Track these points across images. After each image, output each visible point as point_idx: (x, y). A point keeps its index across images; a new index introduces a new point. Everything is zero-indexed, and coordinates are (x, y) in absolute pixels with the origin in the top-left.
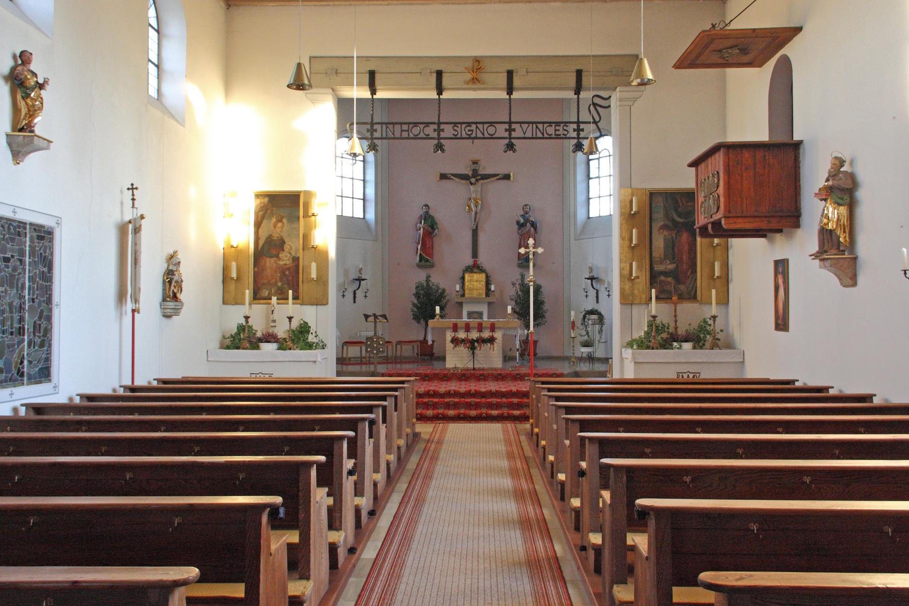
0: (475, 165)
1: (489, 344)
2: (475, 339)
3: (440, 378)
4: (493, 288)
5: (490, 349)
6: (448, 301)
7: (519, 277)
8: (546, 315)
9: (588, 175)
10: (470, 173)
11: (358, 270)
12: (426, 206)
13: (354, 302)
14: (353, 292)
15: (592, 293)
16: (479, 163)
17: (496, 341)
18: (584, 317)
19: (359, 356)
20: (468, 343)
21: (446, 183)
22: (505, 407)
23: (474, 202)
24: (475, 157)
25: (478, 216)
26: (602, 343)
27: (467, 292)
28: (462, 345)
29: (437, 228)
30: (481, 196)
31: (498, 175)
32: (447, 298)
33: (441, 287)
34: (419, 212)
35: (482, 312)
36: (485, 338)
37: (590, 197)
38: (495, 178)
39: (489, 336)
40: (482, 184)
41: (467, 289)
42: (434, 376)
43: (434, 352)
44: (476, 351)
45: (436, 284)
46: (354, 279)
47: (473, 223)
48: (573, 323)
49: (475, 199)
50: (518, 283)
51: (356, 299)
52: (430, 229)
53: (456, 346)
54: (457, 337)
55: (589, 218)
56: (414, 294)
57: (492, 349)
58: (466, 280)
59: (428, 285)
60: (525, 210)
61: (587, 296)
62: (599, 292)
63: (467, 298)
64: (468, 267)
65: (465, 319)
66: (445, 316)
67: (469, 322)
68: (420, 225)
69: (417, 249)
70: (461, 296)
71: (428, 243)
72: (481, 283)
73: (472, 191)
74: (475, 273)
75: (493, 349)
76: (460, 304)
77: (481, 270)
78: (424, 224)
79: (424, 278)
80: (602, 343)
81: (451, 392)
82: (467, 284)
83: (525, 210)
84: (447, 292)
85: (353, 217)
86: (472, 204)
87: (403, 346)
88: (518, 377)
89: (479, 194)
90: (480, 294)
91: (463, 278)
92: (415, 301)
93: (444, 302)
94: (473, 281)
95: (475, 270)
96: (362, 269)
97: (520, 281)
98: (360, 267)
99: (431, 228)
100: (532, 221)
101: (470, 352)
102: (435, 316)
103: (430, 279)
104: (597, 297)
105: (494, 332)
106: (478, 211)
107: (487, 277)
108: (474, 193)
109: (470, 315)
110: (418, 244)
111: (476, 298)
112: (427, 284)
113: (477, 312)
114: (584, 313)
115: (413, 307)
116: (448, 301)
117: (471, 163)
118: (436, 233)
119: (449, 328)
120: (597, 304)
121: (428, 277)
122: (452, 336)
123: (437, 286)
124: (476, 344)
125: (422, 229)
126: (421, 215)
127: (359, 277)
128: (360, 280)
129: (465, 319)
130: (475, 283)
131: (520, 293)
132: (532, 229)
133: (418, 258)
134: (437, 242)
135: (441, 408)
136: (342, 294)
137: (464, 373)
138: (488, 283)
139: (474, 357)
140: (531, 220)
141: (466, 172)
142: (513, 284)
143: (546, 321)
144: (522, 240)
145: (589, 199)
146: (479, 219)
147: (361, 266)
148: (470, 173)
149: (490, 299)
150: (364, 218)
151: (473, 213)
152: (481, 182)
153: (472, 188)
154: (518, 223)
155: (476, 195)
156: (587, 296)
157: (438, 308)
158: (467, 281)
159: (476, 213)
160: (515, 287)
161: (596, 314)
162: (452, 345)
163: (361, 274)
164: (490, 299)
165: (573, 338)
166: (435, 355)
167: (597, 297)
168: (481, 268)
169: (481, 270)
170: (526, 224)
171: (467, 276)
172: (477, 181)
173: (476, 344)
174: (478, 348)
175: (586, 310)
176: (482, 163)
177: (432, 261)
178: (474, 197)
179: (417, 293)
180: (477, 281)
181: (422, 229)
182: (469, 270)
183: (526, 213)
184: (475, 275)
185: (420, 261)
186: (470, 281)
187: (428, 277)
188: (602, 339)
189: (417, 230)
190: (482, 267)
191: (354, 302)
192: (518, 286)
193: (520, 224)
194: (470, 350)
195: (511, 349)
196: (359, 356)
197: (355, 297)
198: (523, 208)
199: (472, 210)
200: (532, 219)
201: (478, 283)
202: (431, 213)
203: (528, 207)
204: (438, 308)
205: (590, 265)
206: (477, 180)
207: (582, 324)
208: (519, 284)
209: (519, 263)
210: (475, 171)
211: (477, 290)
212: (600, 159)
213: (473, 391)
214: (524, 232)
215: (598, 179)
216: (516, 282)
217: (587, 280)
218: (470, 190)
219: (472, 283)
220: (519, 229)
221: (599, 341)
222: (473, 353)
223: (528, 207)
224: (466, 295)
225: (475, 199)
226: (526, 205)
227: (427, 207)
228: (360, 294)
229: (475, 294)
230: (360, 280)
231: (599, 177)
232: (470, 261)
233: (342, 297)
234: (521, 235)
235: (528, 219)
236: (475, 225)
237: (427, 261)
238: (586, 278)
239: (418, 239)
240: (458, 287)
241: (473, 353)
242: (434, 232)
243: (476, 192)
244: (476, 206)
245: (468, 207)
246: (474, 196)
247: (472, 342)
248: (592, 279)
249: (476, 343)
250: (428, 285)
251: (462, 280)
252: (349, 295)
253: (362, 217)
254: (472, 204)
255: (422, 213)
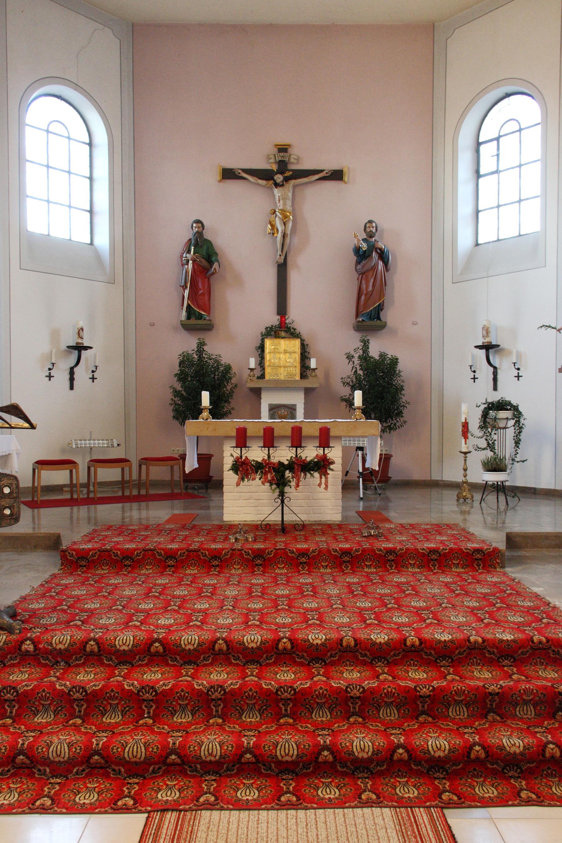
0: (282, 154)
1: (317, 475)
2: (286, 463)
3: (204, 562)
4: (313, 363)
5: (319, 485)
6: (236, 386)
7: (360, 345)
8: (405, 412)
9: (477, 172)
10: (275, 167)
11: (77, 331)
12: (198, 222)
13: (72, 388)
14: (68, 371)
15: (485, 372)
16: (289, 150)
17: (331, 467)
18: (485, 415)
19: (68, 482)
20: (269, 471)
21: (233, 186)
22: (388, 705)
23: (280, 216)
24: (283, 140)
25: (288, 240)
26: (518, 462)
27: (268, 370)
28: (258, 477)
29: (218, 261)
30: (294, 209)
31: (322, 171)
32: (234, 381)
33: (222, 362)
34: (187, 234)
35: (295, 405)
36: (308, 459)
37: (480, 209)
38: (317, 177)
39: (317, 455)
40: (295, 187)
41: (269, 366)
42: (188, 556)
43: (211, 475)
44: (287, 489)
45: (213, 357)
46: (68, 347)
47: (279, 253)
48: (465, 425)
49: (283, 211)
50: (356, 356)
51: (75, 383)
52: (204, 263)
53: (243, 479)
54: (246, 457)
55: (477, 245)
56: (176, 375)
57: (323, 486)
58: (267, 350)
59: (200, 357)
60: (368, 230)
61: (474, 378)
62: (499, 371)
63: (268, 381)
64: (271, 328)
65: (265, 417)
66: (230, 413)
67: (273, 426)
68: (188, 255)
69: (184, 296)
70: (258, 378)
71: (200, 286)
72: (294, 356)
73: (277, 197)
74: (282, 338)
75: (327, 486)
76: (257, 392)
77: (292, 334)
78: (194, 254)
79: (194, 346)
80: (518, 462)
81: (217, 647)
82: (268, 357)
83: (368, 230)
84: (234, 369)
85: (70, 240)
86: (277, 220)
87: (151, 468)
88: (391, 557)
89: (289, 203)
90: (291, 375)
91: (262, 348)
92: (178, 387)
93: (229, 388)
94: (280, 353)
95: (283, 334)
96: (82, 329)
97: (361, 352)
98: (80, 327)
99: (207, 261)
100: (380, 249)
101: (274, 491)
102: (200, 411)
103: (206, 348)
104: (495, 380)
105: (328, 447)
106: (288, 232)
107: (304, 347)
108: (281, 201)
109: (274, 410)
110: (185, 287)
111: (284, 381)
112: (199, 357)
113: (284, 406)
114: (483, 407)
115: (174, 396)
116: (236, 386)
117: (276, 150)
118: (215, 269)
119: (228, 437)
120: (495, 392)
121: (201, 345)
122: (235, 455)
123: (217, 362)
124: (288, 474)
125: (191, 262)
126: (191, 239)
127: (77, 343)
128: (79, 348)
129: (265, 417)
130: (282, 356)
131: (360, 372)
132: (381, 263)
133: (184, 313)
134: (218, 289)
135: (183, 709)
136: (48, 374)
137: (259, 550)
138: (304, 356)
139: (283, 502)
140: (379, 246)
141: (268, 167)
142: (347, 357)
143: (405, 422)
144: (364, 282)
145: (477, 212)
146: (289, 246)
147: (81, 324)
148: (275, 167)
149: (307, 383)
150: (92, 244)
151: (279, 236)
152: (293, 182)
153: (277, 192)
154: (357, 250)
155: (285, 204)
156: (474, 378)
157: (205, 397)
158: (269, 353)
159: (284, 236)
160: (351, 363)
161: (507, 410)
162: (236, 478)
163: (82, 338)
164: (307, 383)
165: (465, 453)
166: (213, 479)
167: (495, 380)
168: (292, 330)
169: (292, 334)
170: (370, 256)
171: (269, 344)
172: (286, 181)
173: (288, 474)
174: (293, 484)
175: (488, 401)
176: (295, 152)
177: (207, 318)
178: (281, 207)
179: (182, 372)
180: (285, 352)
181: (191, 262)
182: (273, 333)
183: (371, 235)
184: (282, 341)
185: (189, 317)
186: (275, 352)
187: (201, 345)
188: (517, 456)
189: (183, 265)
190: (295, 329)
191: (72, 388)
192: (356, 360)
193: (361, 253)
194: (274, 486)
195: (347, 472)
196: (68, 482)
197: (72, 379)
198: (365, 226)
199: (278, 230)
200: (381, 245)
201: (288, 355)
202: (207, 235)
203: (374, 225)
204: (205, 397)
205: (485, 323)
206: (287, 179)
207: (481, 427)
208: (359, 357)
209: (359, 322)
210: (283, 166)
211: (285, 367)
212: (501, 139)
213: (285, 643)
214: (366, 268)
215: (496, 175)
216: (352, 353)
217: (478, 350)
218: (274, 196)
219: (277, 355)
220: (358, 263)
221: (513, 460)
222: (282, 494)
223: (374, 225)
224: (267, 377)
225: (283, 211)
226: (370, 222)
227: (200, 225)
228: (81, 373)
229: (282, 375)
230: (79, 348)
231: (497, 172)
232: (274, 320)
233: (48, 378)
234: (363, 274)
235: (374, 245)
236: (283, 257)
237: (200, 317)
238: (476, 347)
239: (183, 281)
240: (252, 363)
241: (282, 494)
242: (211, 267)
243: (285, 199)
244: (285, 224)
245: (272, 225)
246: (280, 205)
247: (280, 468)
248: (488, 347)
249: (287, 472)
250: (200, 357)
251: (260, 350)
252: (62, 377)
253: (89, 242)
254: (277, 220)
255: (191, 237)
